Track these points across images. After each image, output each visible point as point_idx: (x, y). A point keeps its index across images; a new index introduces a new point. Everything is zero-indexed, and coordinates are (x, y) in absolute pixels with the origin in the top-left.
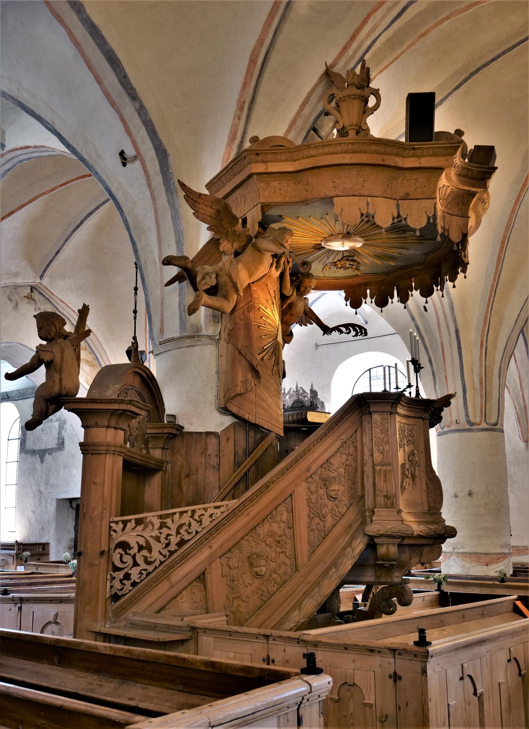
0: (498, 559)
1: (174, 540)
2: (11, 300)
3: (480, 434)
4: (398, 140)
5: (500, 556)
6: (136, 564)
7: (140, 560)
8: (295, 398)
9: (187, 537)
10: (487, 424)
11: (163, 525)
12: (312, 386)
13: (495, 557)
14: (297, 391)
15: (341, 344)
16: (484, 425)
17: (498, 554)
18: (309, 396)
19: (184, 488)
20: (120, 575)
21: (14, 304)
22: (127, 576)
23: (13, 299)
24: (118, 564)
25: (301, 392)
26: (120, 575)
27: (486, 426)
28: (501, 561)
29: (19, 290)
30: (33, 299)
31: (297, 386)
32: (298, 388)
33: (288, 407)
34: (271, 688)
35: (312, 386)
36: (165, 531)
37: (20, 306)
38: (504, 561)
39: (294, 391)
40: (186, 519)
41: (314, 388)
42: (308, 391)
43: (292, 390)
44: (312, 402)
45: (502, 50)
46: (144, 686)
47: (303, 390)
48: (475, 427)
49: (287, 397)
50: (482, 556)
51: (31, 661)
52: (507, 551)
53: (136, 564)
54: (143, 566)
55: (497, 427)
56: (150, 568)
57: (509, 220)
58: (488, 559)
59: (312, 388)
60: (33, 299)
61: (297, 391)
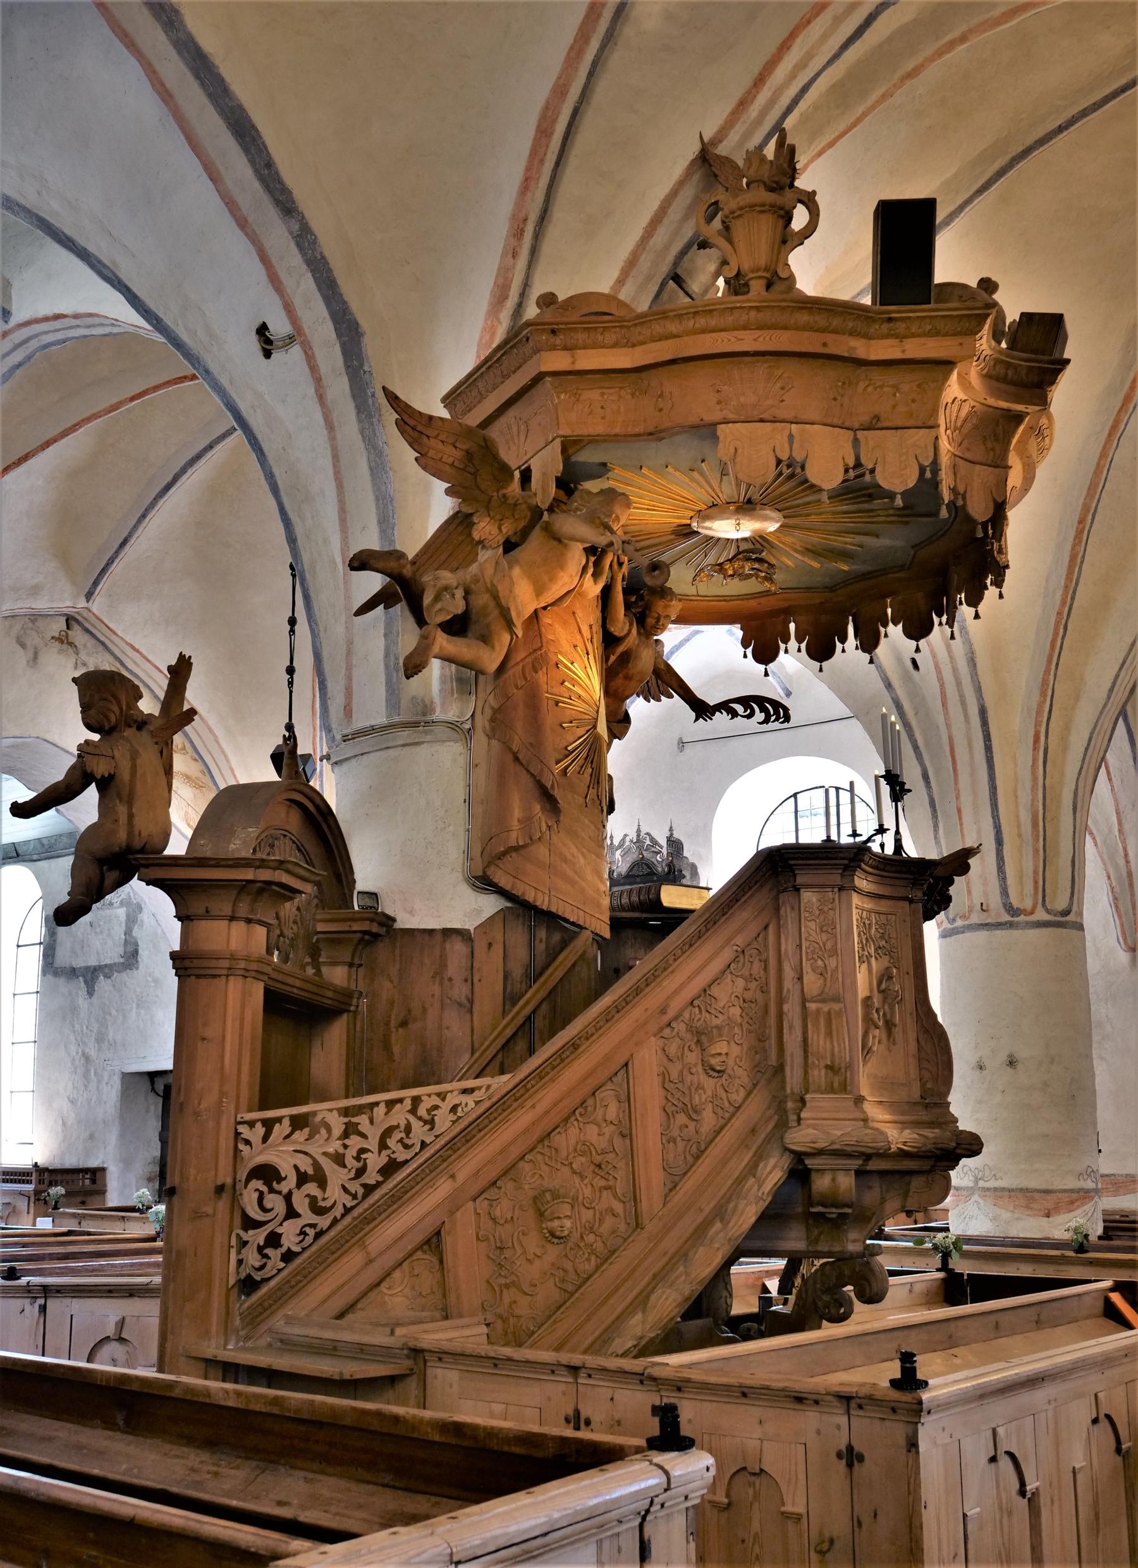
0: (1072, 1202)
1: (375, 1161)
2: (23, 645)
3: (1033, 933)
4: (857, 300)
5: (1075, 1196)
6: (292, 1213)
7: (300, 1203)
8: (634, 856)
9: (402, 1155)
10: (1048, 911)
11: (350, 1130)
12: (671, 829)
13: (1065, 1197)
14: (638, 841)
15: (734, 741)
16: (1041, 915)
17: (1072, 1191)
18: (664, 851)
19: (396, 1049)
20: (258, 1237)
21: (31, 654)
22: (274, 1240)
23: (29, 643)
24: (255, 1213)
25: (648, 842)
26: (258, 1237)
27: (1046, 917)
28: (1078, 1207)
29: (40, 623)
30: (71, 644)
31: (639, 831)
32: (642, 834)
33: (620, 874)
34: (582, 1479)
35: (671, 829)
36: (355, 1142)
37: (43, 659)
38: (1085, 1207)
39: (631, 841)
40: (400, 1116)
41: (676, 835)
42: (663, 842)
43: (628, 839)
44: (670, 865)
45: (1081, 108)
46: (310, 1476)
47: (652, 839)
48: (1022, 918)
49: (618, 854)
50: (1037, 1195)
51: (67, 1421)
52: (1090, 1185)
53: (292, 1213)
54: (308, 1217)
55: (1068, 918)
56: (323, 1222)
57: (1095, 472)
58: (1049, 1202)
59: (671, 835)
60: (71, 644)
61: (639, 841)
